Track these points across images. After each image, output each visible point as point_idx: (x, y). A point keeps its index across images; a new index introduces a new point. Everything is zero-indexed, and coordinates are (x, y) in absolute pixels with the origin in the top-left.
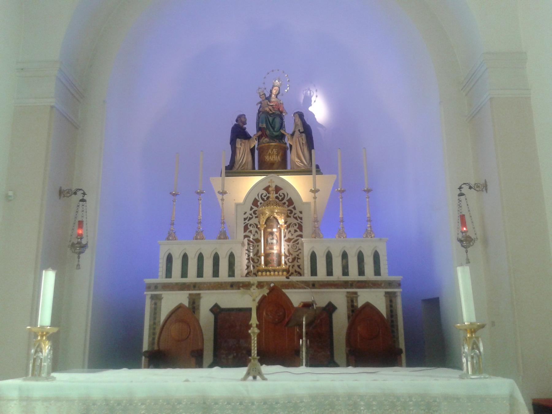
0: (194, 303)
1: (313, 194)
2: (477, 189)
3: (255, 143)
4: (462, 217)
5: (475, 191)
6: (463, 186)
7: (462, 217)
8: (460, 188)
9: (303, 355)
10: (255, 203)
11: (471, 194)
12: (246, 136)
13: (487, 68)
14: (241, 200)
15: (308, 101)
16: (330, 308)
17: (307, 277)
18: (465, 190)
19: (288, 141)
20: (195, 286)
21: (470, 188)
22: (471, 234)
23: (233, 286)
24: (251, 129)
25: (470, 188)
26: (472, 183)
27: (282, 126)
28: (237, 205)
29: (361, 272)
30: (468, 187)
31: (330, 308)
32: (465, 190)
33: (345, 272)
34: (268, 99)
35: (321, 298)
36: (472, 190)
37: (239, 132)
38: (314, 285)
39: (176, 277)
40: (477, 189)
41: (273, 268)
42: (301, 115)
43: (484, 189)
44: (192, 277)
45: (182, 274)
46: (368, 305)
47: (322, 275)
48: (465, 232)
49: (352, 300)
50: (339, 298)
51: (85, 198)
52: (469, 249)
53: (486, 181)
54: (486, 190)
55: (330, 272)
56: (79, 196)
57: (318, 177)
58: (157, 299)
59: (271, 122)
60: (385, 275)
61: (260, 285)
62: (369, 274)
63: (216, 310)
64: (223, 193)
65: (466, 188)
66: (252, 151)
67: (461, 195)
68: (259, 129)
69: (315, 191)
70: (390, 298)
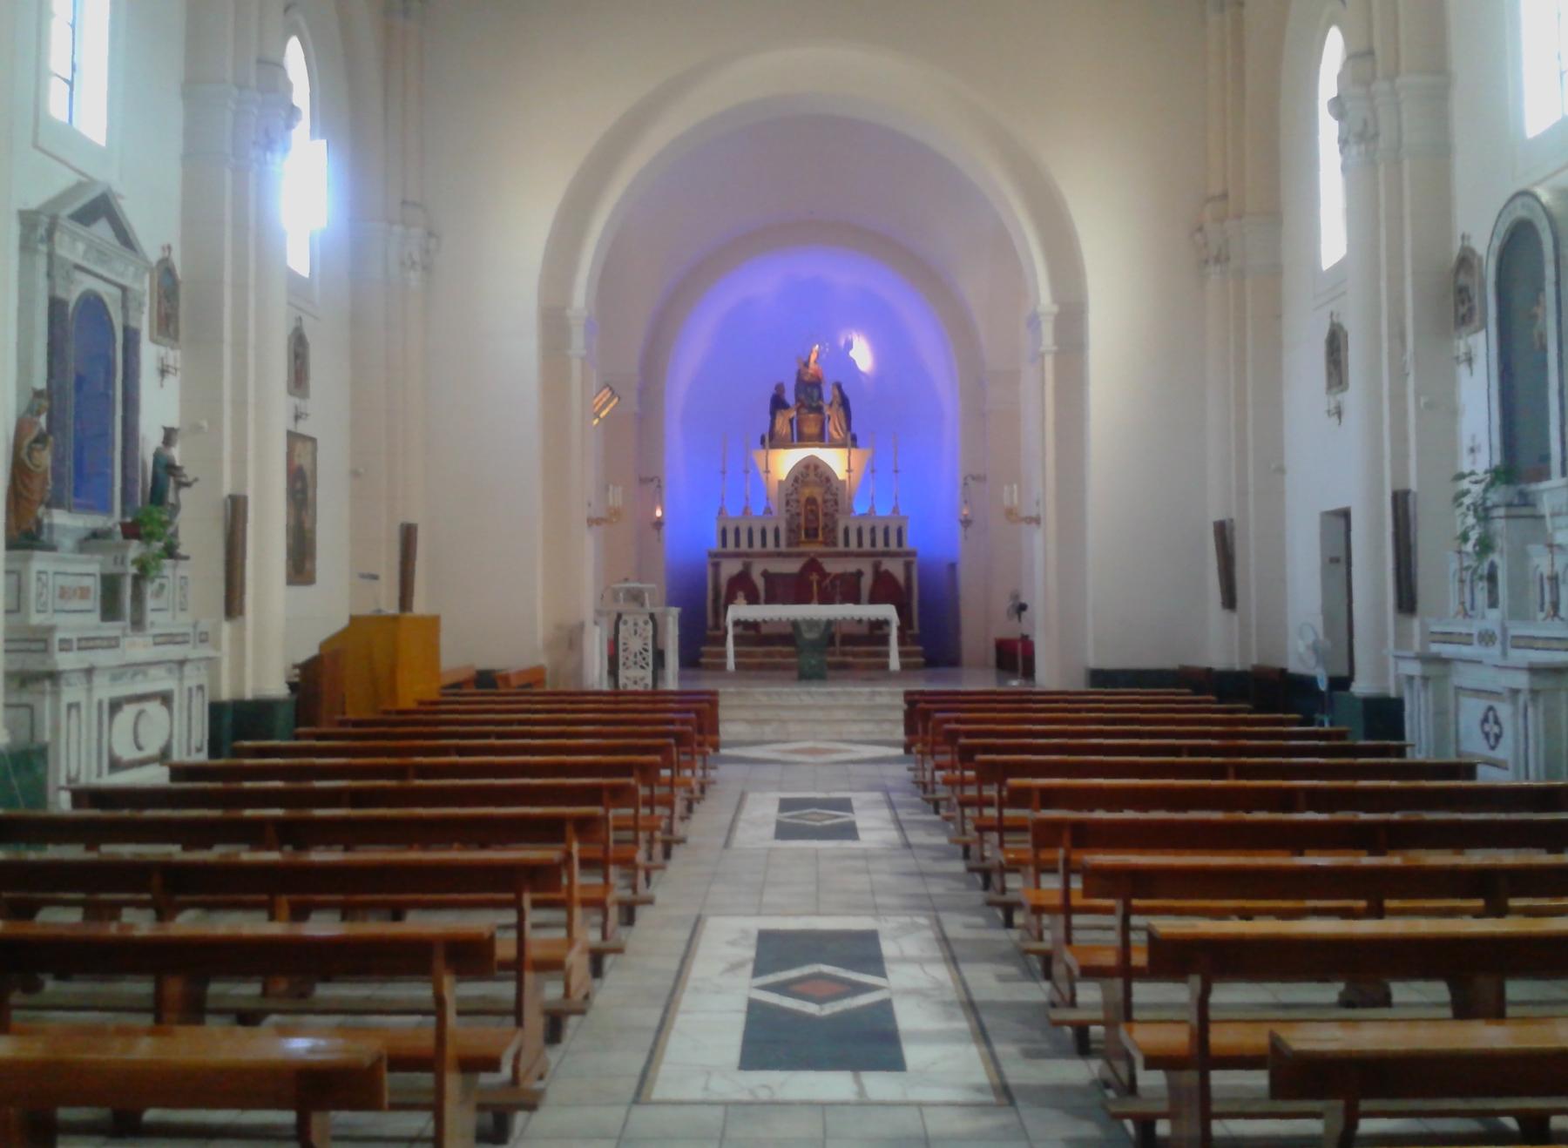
0: (747, 567)
3: (793, 414)
10: (796, 480)
11: (971, 483)
12: (785, 406)
14: (783, 477)
15: (849, 345)
16: (859, 574)
17: (841, 547)
19: (827, 412)
20: (746, 555)
23: (780, 555)
24: (790, 397)
27: (820, 397)
28: (780, 482)
29: (887, 543)
31: (859, 574)
33: (873, 544)
34: (807, 364)
35: (850, 566)
37: (778, 403)
38: (780, 555)
39: (731, 547)
42: (839, 386)
44: (744, 546)
46: (887, 572)
47: (853, 545)
49: (876, 567)
50: (866, 567)
55: (860, 544)
56: (656, 482)
57: (853, 451)
58: (716, 566)
59: (809, 388)
60: (907, 546)
61: (799, 555)
62: (893, 546)
63: (765, 574)
64: (767, 472)
66: (791, 421)
68: (798, 400)
69: (849, 471)
70: (908, 566)
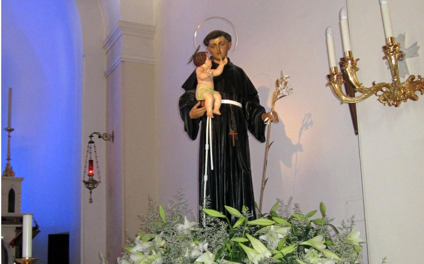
1: (7, 133)
2: (105, 138)
4: (91, 162)
5: (103, 140)
6: (94, 135)
7: (91, 162)
8: (91, 136)
9: (28, 252)
13: (122, 34)
18: (95, 138)
21: (100, 137)
22: (95, 178)
25: (100, 137)
26: (102, 133)
30: (98, 136)
32: (95, 138)
36: (101, 139)
40: (105, 138)
41: (303, 256)
43: (111, 139)
45: (252, 246)
48: (92, 175)
51: (92, 140)
52: (93, 191)
53: (113, 133)
54: (113, 139)
65: (96, 136)
67: (91, 142)
